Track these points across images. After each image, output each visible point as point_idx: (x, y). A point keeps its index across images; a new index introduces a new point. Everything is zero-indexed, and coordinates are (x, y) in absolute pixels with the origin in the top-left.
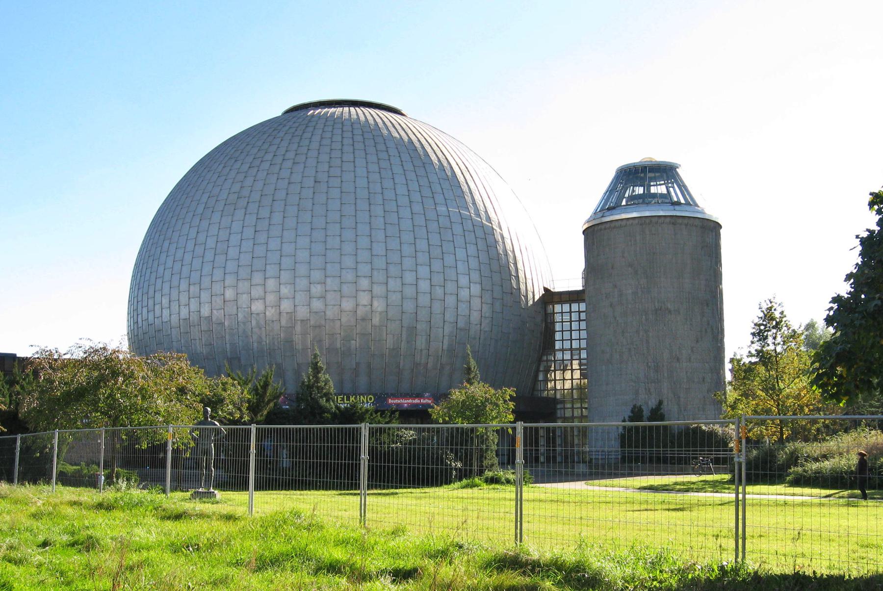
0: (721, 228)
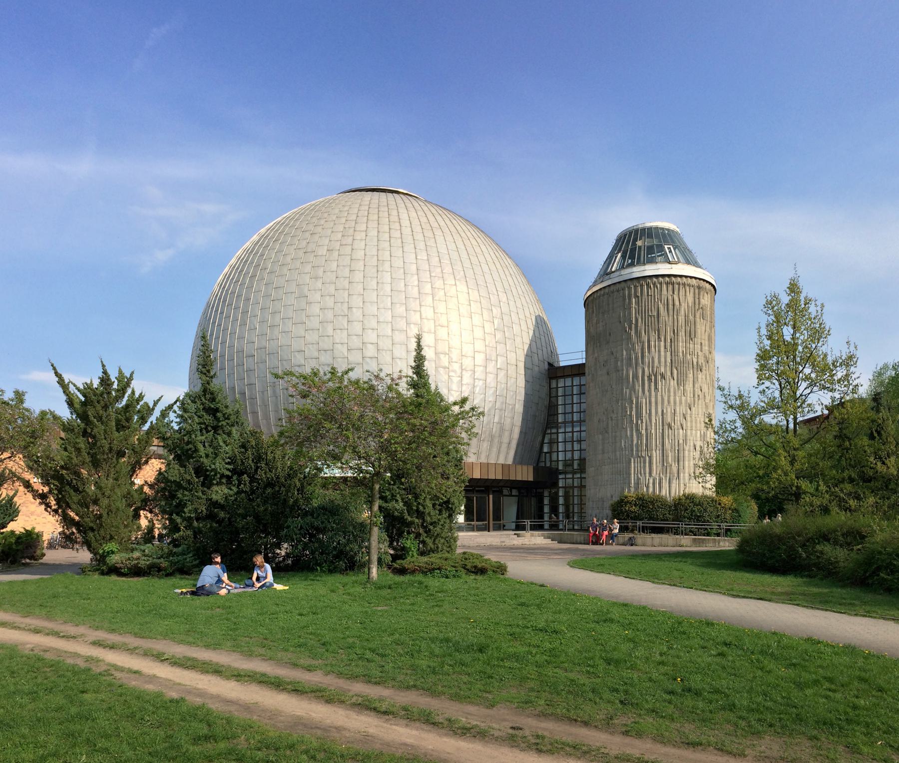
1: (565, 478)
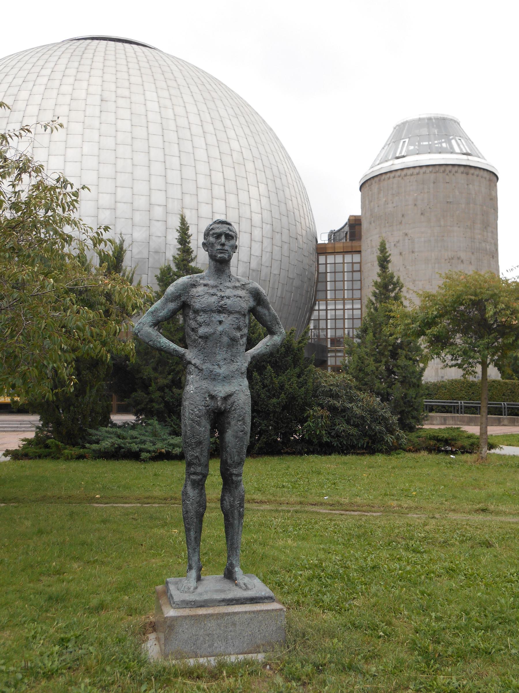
1: (336, 357)
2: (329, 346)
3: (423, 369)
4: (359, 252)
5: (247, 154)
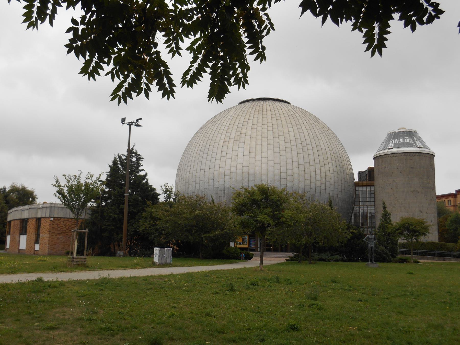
0: (434, 156)
2: (361, 226)
3: (398, 240)
4: (374, 186)
5: (328, 150)
